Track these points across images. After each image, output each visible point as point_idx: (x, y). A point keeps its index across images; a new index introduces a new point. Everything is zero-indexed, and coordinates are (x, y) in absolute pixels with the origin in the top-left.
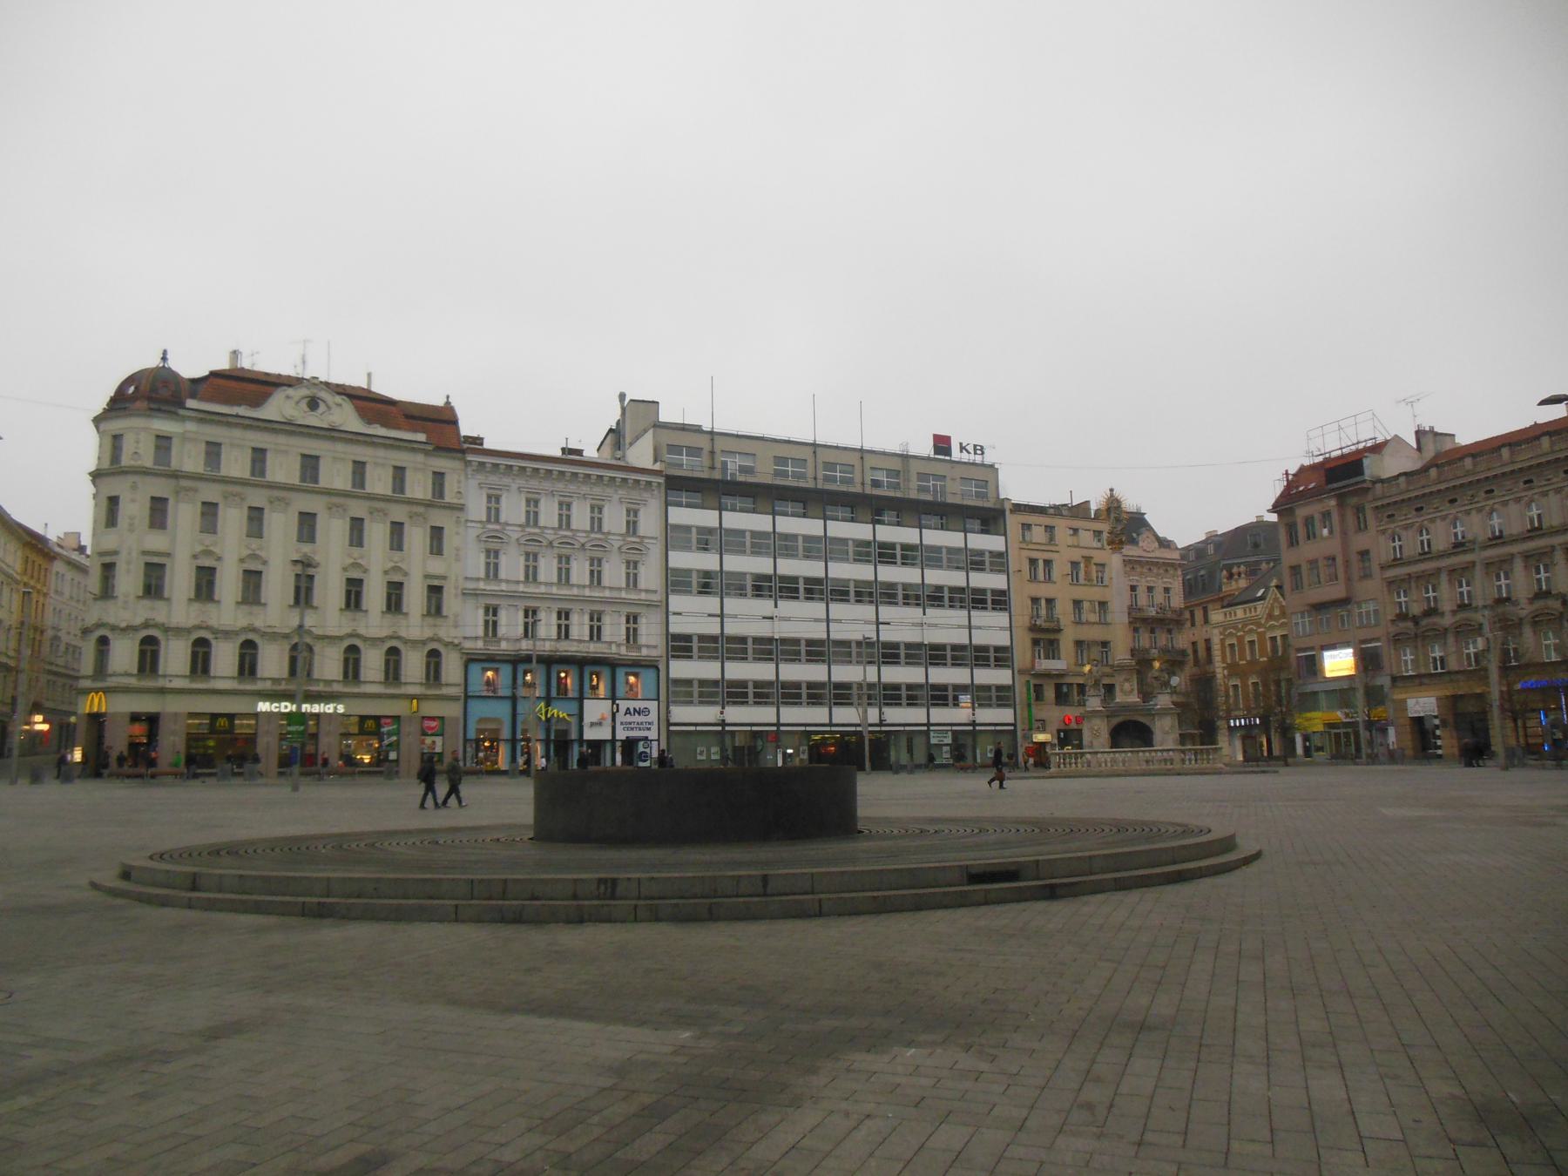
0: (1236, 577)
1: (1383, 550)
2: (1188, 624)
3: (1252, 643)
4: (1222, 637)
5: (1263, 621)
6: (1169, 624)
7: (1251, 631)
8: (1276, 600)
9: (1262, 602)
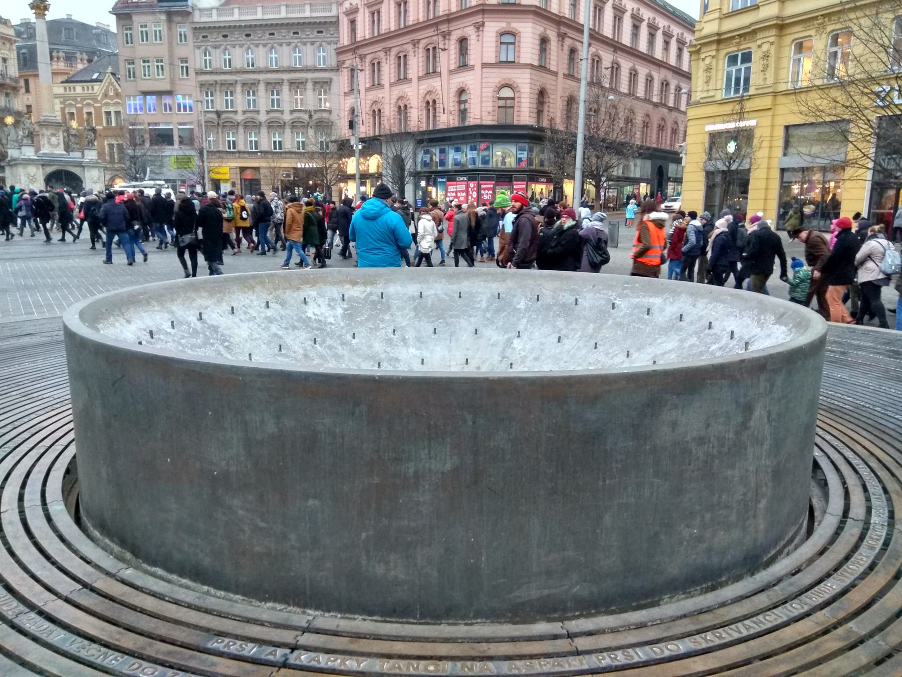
0: (56, 59)
1: (197, 60)
2: (23, 90)
3: (89, 114)
4: (63, 106)
5: (99, 98)
6: (7, 89)
7: (70, 105)
8: (111, 83)
9: (99, 83)
